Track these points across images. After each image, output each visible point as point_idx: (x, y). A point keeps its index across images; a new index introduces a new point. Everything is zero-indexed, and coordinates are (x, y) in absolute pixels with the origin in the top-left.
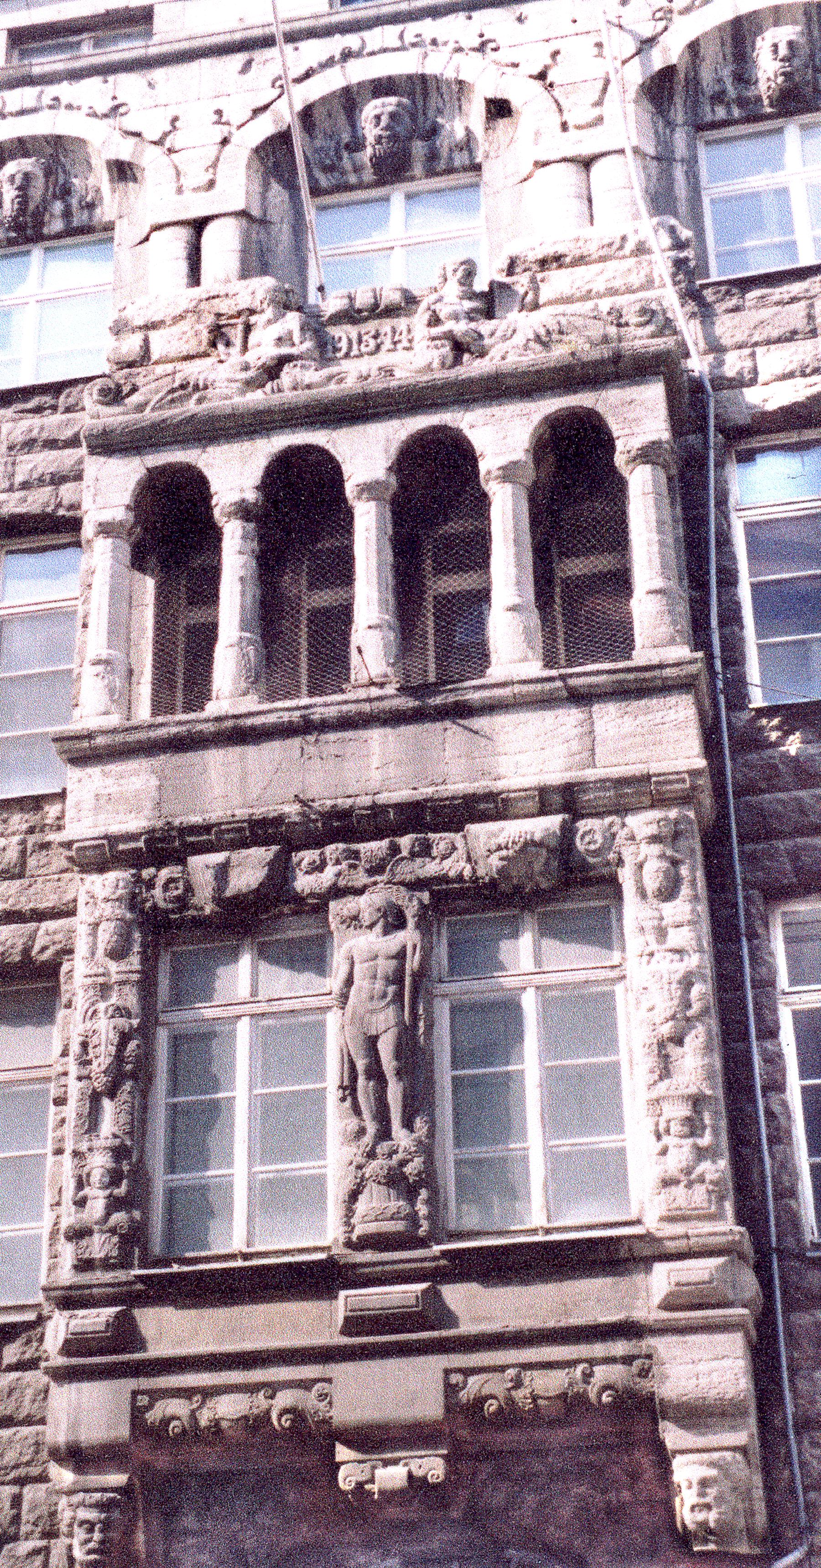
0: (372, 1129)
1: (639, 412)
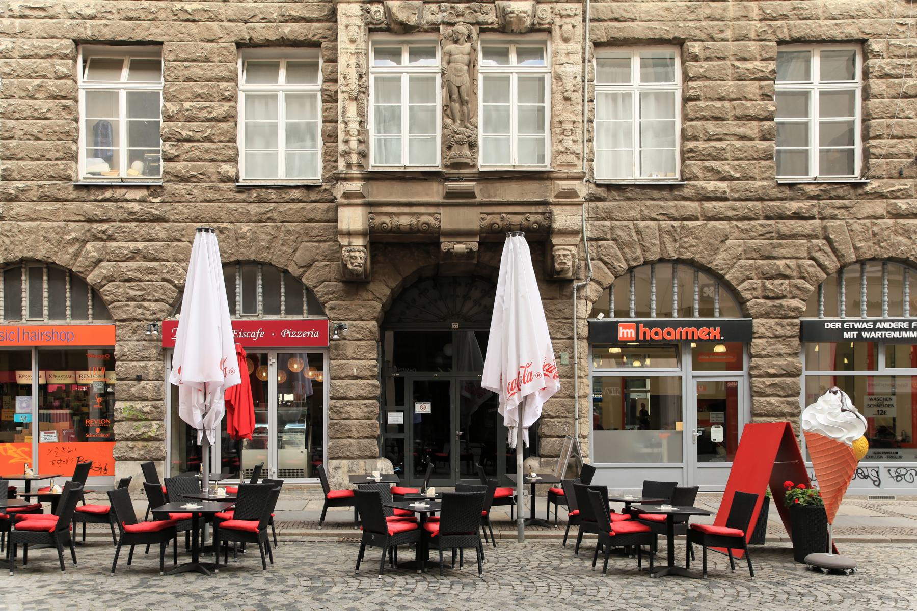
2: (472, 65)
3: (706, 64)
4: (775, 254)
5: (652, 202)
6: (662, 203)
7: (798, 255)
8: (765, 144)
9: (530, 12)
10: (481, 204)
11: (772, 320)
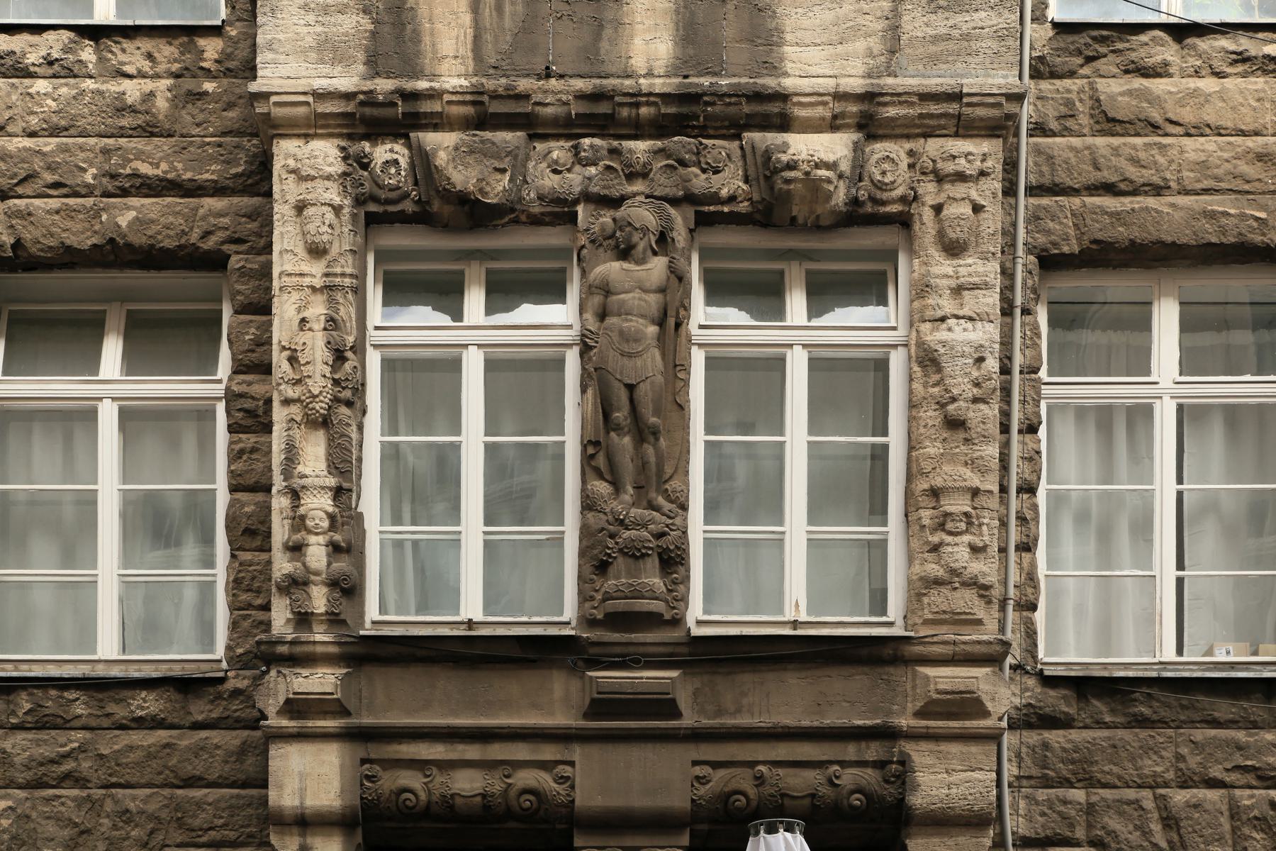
5: (1213, 732)
9: (845, 167)
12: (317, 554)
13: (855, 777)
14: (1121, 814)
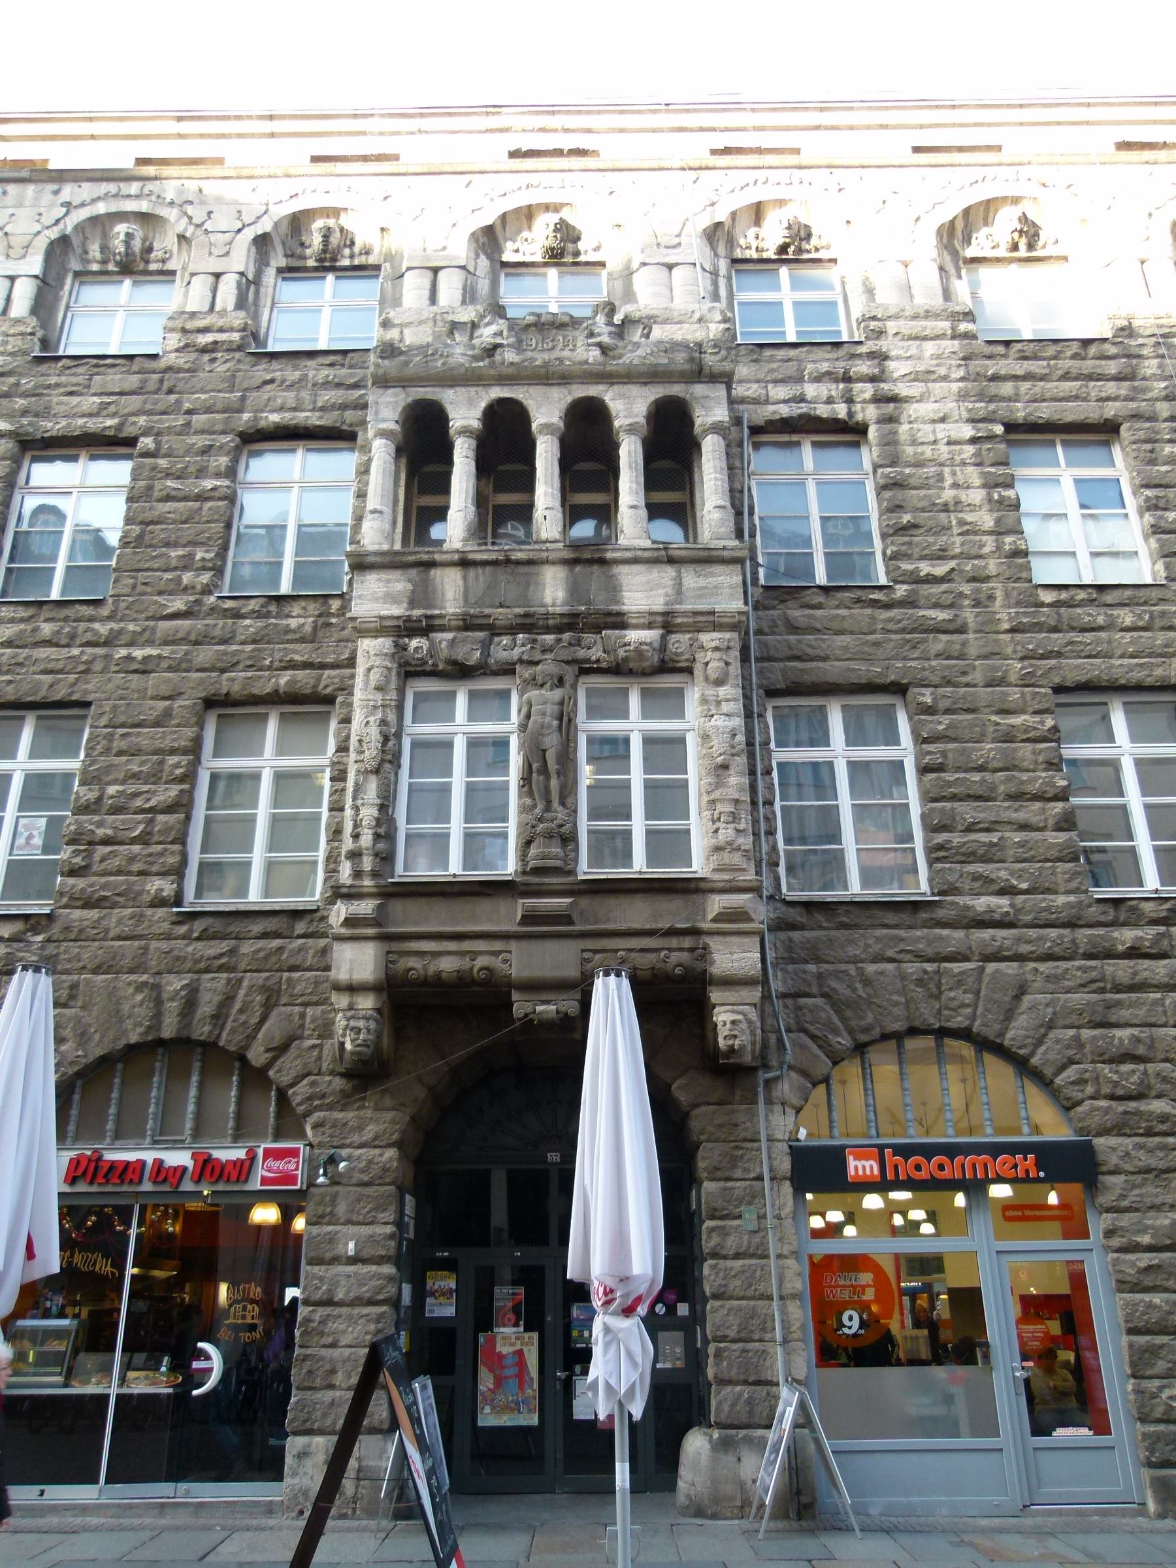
0: (540, 807)
1: (712, 403)
2: (565, 719)
3: (946, 719)
4: (1113, 1019)
5: (885, 931)
6: (902, 933)
7: (1153, 1020)
8: (1062, 837)
9: (656, 645)
10: (583, 935)
11: (1128, 1141)
12: (366, 840)
13: (676, 957)
14: (838, 978)
